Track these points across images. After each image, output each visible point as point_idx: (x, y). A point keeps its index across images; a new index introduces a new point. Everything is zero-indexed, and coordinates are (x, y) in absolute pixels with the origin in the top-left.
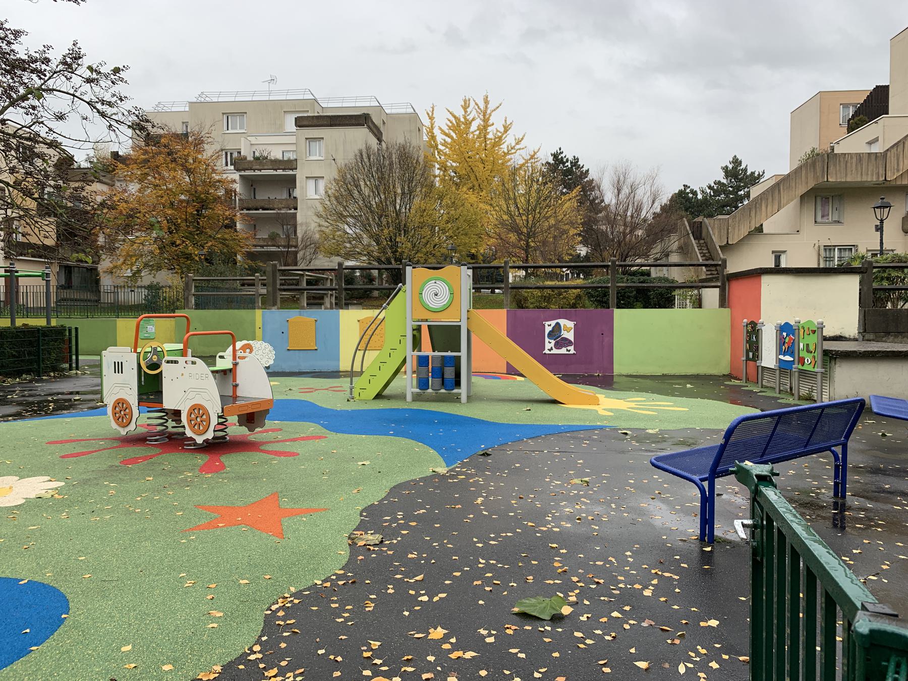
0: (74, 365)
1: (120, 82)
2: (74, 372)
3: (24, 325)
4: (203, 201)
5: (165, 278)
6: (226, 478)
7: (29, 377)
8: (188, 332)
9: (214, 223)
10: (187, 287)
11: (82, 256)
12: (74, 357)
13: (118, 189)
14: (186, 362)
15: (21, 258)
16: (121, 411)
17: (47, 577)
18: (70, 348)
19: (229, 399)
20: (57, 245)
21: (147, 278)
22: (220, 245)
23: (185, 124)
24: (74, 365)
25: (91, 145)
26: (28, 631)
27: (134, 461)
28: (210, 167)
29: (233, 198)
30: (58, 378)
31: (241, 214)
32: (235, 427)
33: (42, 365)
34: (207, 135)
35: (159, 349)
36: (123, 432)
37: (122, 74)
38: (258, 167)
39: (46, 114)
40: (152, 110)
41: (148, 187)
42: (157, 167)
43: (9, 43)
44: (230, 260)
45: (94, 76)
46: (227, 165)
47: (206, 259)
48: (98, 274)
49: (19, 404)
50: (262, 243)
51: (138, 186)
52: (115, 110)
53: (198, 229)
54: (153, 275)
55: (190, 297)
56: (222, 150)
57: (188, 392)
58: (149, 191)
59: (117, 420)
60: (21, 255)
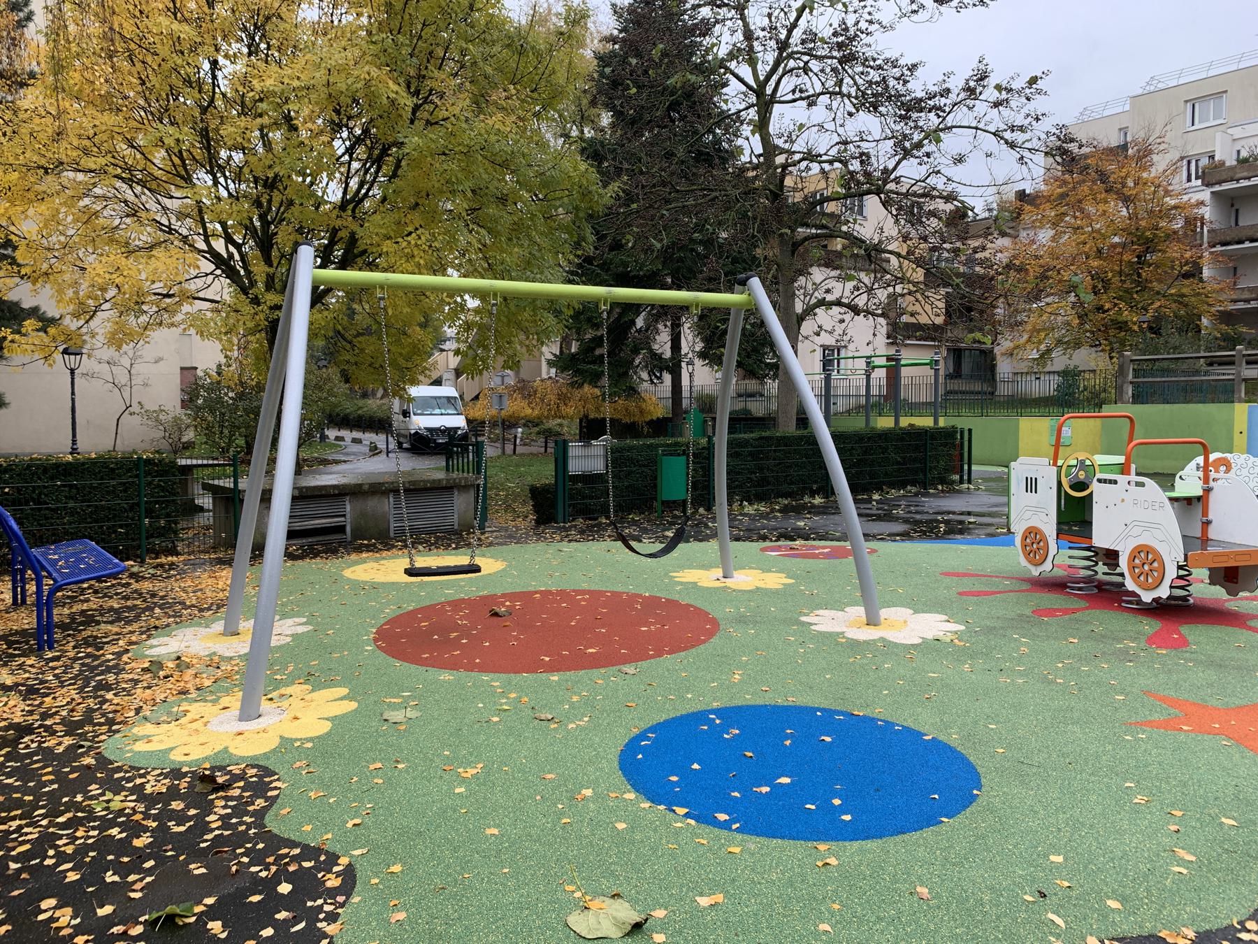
0: (966, 477)
1: (1038, 96)
2: (966, 486)
3: (911, 425)
4: (1149, 241)
5: (1087, 358)
6: (1191, 661)
7: (914, 490)
8: (1131, 440)
9: (1166, 272)
10: (1121, 371)
11: (978, 335)
12: (966, 467)
13: (1024, 241)
14: (1129, 483)
15: (908, 342)
16: (1144, 564)
17: (953, 738)
18: (962, 455)
19: (1197, 541)
20: (946, 323)
21: (1059, 361)
22: (1174, 305)
23: (1124, 131)
24: (966, 477)
25: (994, 190)
26: (936, 796)
27: (1050, 612)
28: (1161, 188)
29: (1198, 230)
30: (948, 492)
31: (1211, 253)
32: (1202, 585)
33: (929, 475)
34: (1159, 140)
35: (1088, 462)
36: (1035, 572)
37: (1040, 84)
38: (1245, 174)
39: (943, 160)
40: (1074, 121)
41: (1065, 232)
42: (1080, 201)
43: (906, 82)
44: (1190, 325)
45: (1004, 95)
46: (1189, 180)
47: (1150, 329)
48: (994, 359)
49: (906, 521)
50: (1246, 295)
51: (1051, 233)
52: (1027, 136)
53: (1139, 284)
54: (1068, 356)
55: (1125, 385)
56: (1182, 158)
57: (1130, 527)
58: (1067, 237)
59: (1027, 555)
60: (909, 338)
